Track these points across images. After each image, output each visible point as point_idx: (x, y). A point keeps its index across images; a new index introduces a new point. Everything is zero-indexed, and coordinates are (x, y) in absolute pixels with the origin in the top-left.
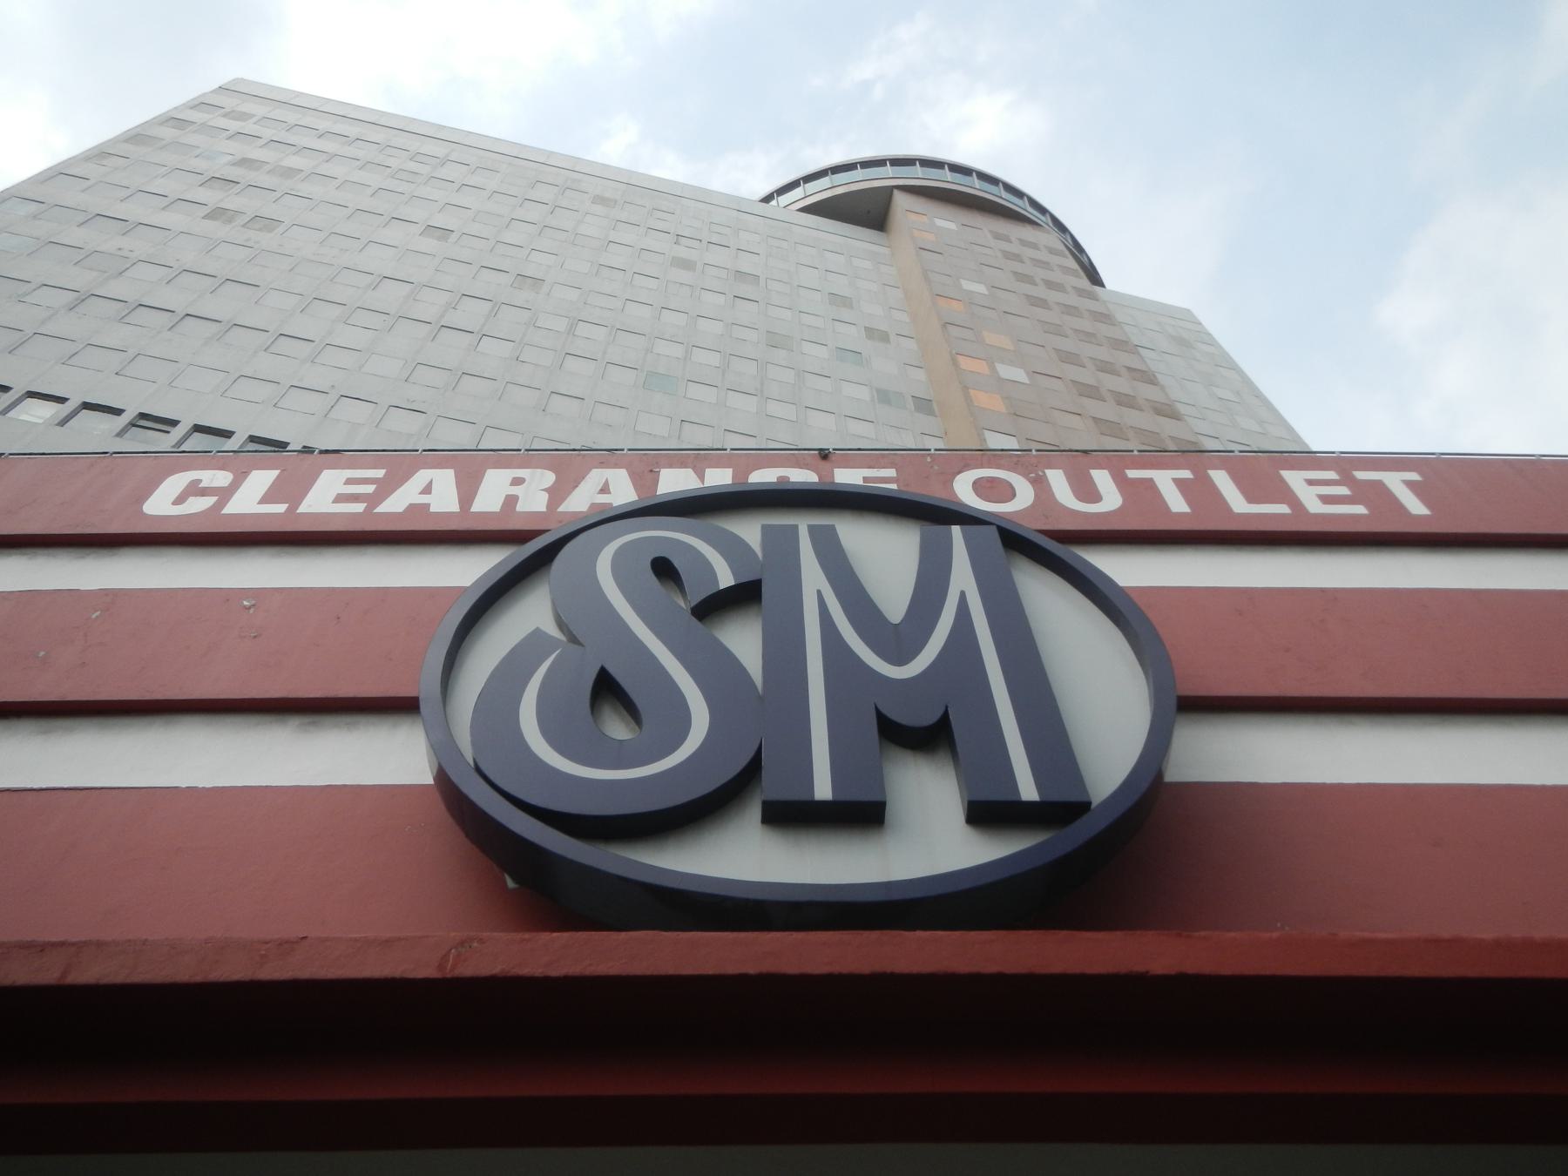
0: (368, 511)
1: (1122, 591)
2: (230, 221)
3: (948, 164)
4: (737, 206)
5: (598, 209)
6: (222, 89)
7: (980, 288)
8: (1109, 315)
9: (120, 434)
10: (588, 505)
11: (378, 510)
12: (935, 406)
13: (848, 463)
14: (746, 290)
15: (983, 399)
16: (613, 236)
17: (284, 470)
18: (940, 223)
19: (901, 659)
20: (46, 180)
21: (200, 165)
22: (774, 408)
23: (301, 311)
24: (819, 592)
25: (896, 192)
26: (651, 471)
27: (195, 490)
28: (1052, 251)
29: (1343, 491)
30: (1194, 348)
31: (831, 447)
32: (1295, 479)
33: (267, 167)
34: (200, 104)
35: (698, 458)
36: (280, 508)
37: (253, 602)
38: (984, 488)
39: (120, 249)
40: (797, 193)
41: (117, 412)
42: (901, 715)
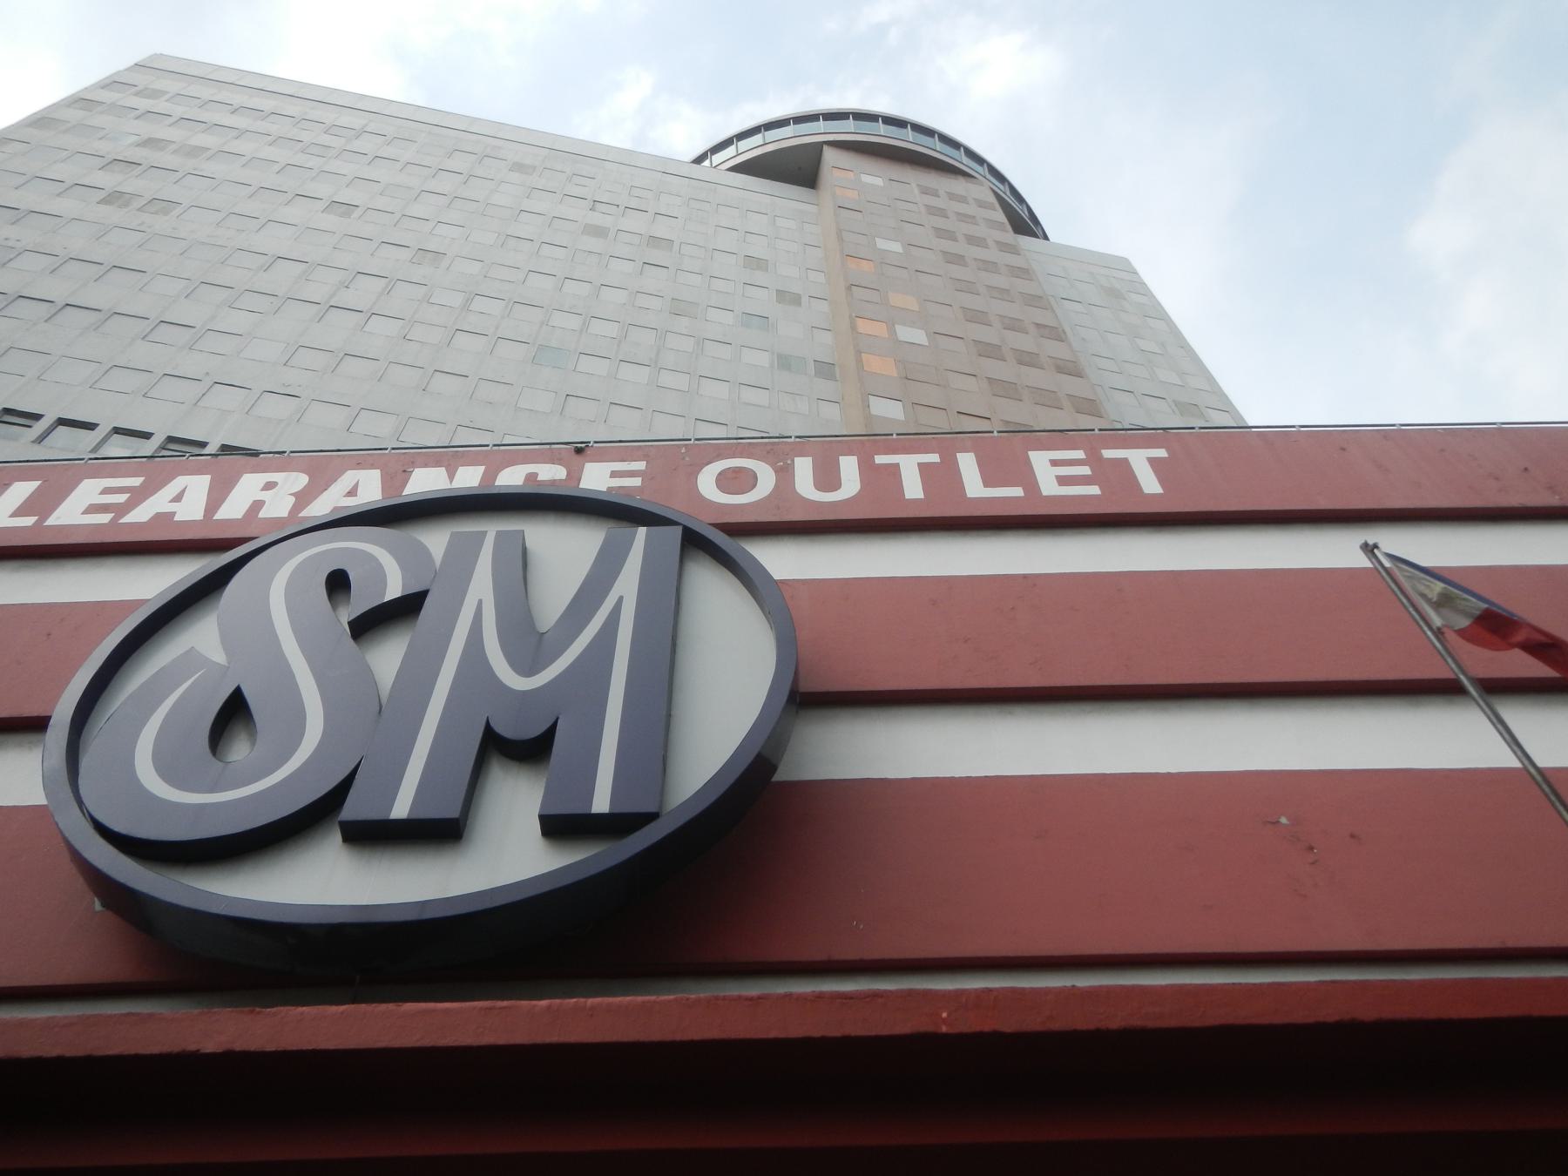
2: (126, 205)
3: (911, 123)
4: (665, 168)
5: (516, 177)
7: (896, 247)
8: (1027, 270)
12: (837, 370)
13: (602, 457)
15: (874, 364)
17: (45, 481)
18: (866, 179)
19: (528, 671)
21: (103, 147)
22: (667, 379)
23: (186, 297)
24: (480, 602)
25: (825, 148)
26: (404, 471)
28: (982, 204)
29: (1085, 470)
30: (1125, 299)
32: (1040, 461)
33: (173, 147)
34: (111, 83)
35: (449, 456)
36: (29, 521)
38: (727, 481)
39: (6, 239)
40: (730, 151)
42: (504, 729)
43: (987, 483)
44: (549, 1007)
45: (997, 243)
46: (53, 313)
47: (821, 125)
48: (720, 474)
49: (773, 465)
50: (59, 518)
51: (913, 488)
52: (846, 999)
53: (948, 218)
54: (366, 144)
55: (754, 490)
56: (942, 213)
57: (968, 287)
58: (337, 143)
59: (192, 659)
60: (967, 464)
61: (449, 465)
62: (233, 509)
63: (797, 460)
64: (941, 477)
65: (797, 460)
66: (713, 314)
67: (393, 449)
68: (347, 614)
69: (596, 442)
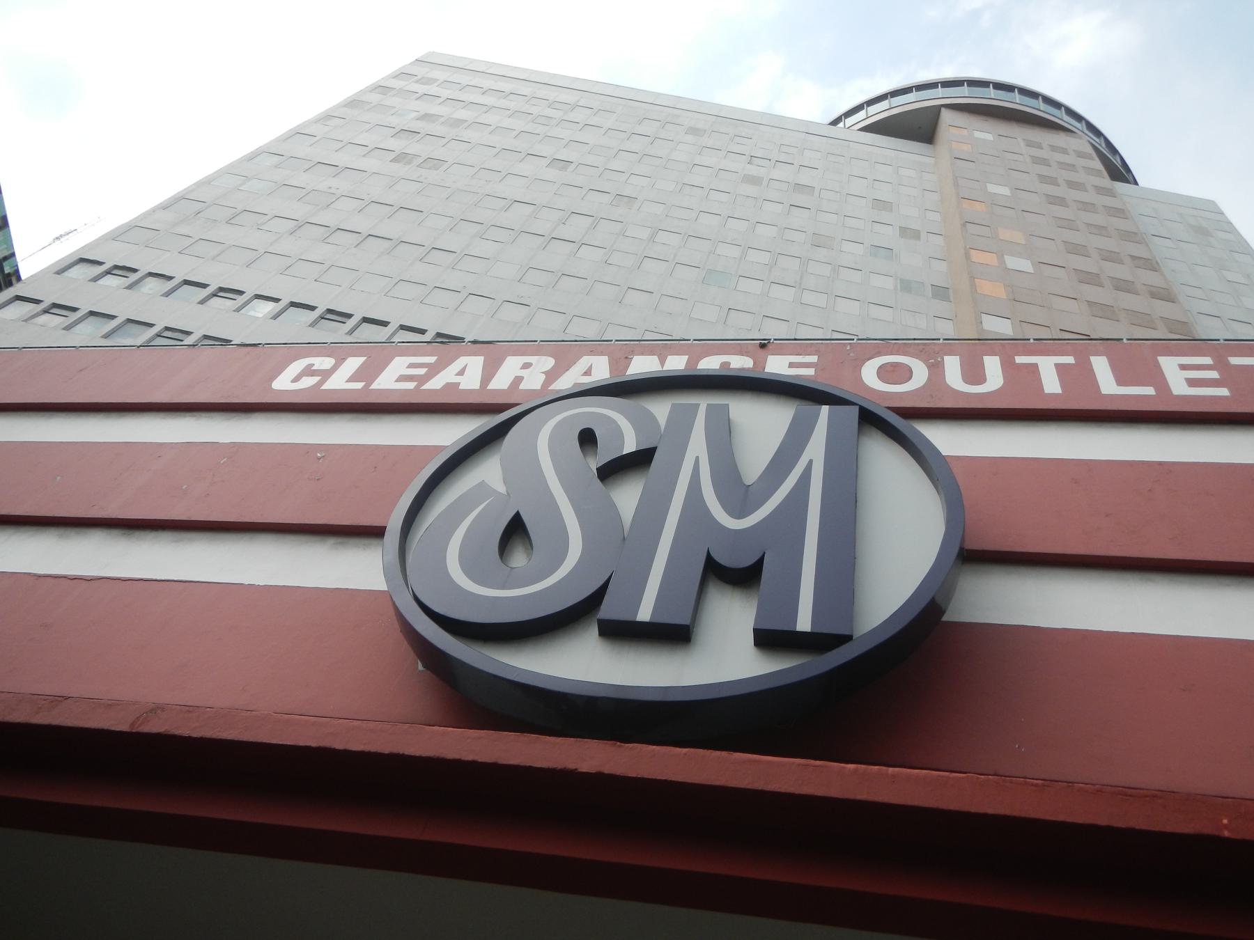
0: (417, 388)
1: (944, 459)
2: (409, 163)
4: (807, 130)
5: (690, 138)
6: (418, 61)
7: (1005, 191)
8: (1123, 210)
9: (313, 324)
10: (573, 383)
11: (423, 388)
13: (781, 351)
14: (801, 199)
15: (986, 287)
16: (698, 160)
18: (978, 134)
19: (739, 514)
20: (287, 139)
21: (394, 121)
22: (808, 298)
24: (697, 458)
25: (943, 110)
26: (626, 358)
27: (309, 371)
28: (1081, 155)
29: (1214, 375)
31: (772, 338)
32: (1170, 366)
33: (442, 120)
34: (402, 74)
35: (662, 347)
36: (359, 385)
37: (323, 454)
38: (887, 373)
39: (330, 188)
40: (861, 115)
41: (312, 308)
42: (722, 558)
43: (1120, 382)
44: (856, 771)
45: (1096, 187)
46: (361, 240)
47: (940, 91)
48: (880, 367)
49: (925, 362)
50: (379, 384)
51: (1051, 384)
52: (1126, 796)
53: (1050, 166)
54: (579, 115)
55: (910, 381)
56: (1045, 162)
57: (1070, 225)
58: (557, 114)
59: (482, 490)
60: (1101, 366)
61: (661, 354)
62: (501, 381)
63: (946, 358)
64: (1076, 375)
65: (946, 358)
66: (847, 247)
67: (617, 341)
68: (594, 464)
69: (775, 340)
